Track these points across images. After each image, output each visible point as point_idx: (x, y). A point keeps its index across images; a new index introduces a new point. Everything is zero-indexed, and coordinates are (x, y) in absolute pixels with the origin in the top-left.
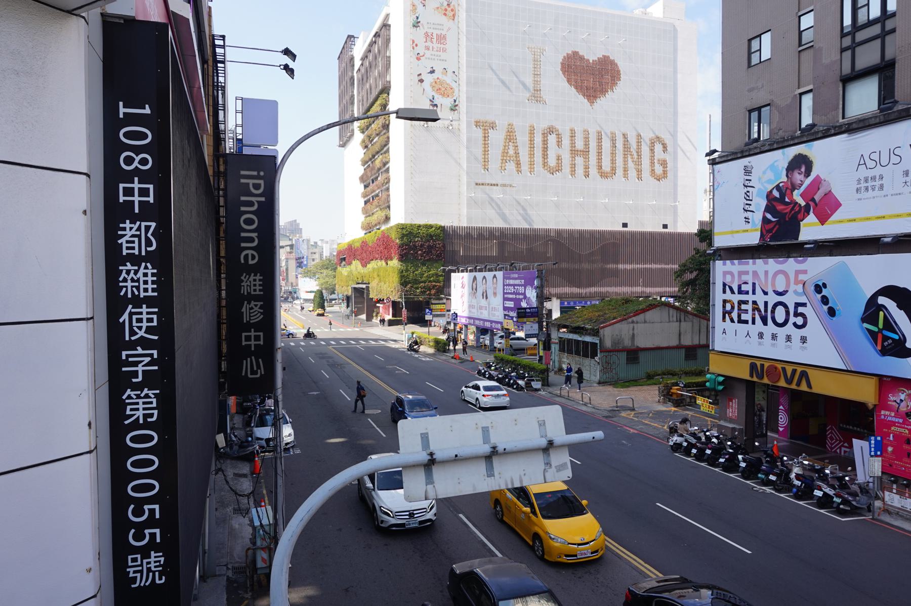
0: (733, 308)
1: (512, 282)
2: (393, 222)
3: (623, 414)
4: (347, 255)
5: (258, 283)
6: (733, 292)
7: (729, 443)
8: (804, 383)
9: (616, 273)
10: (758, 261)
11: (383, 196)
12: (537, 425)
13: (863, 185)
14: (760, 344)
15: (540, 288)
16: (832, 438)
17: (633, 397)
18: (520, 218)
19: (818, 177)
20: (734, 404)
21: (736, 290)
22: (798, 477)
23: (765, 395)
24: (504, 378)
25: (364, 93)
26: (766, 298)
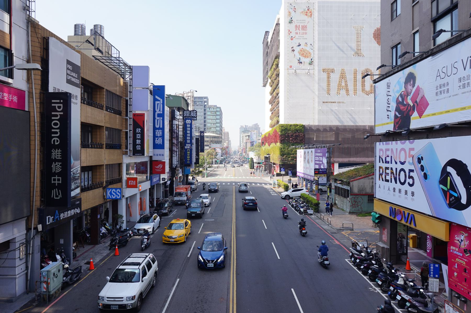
5: (59, 153)
18: (348, 120)
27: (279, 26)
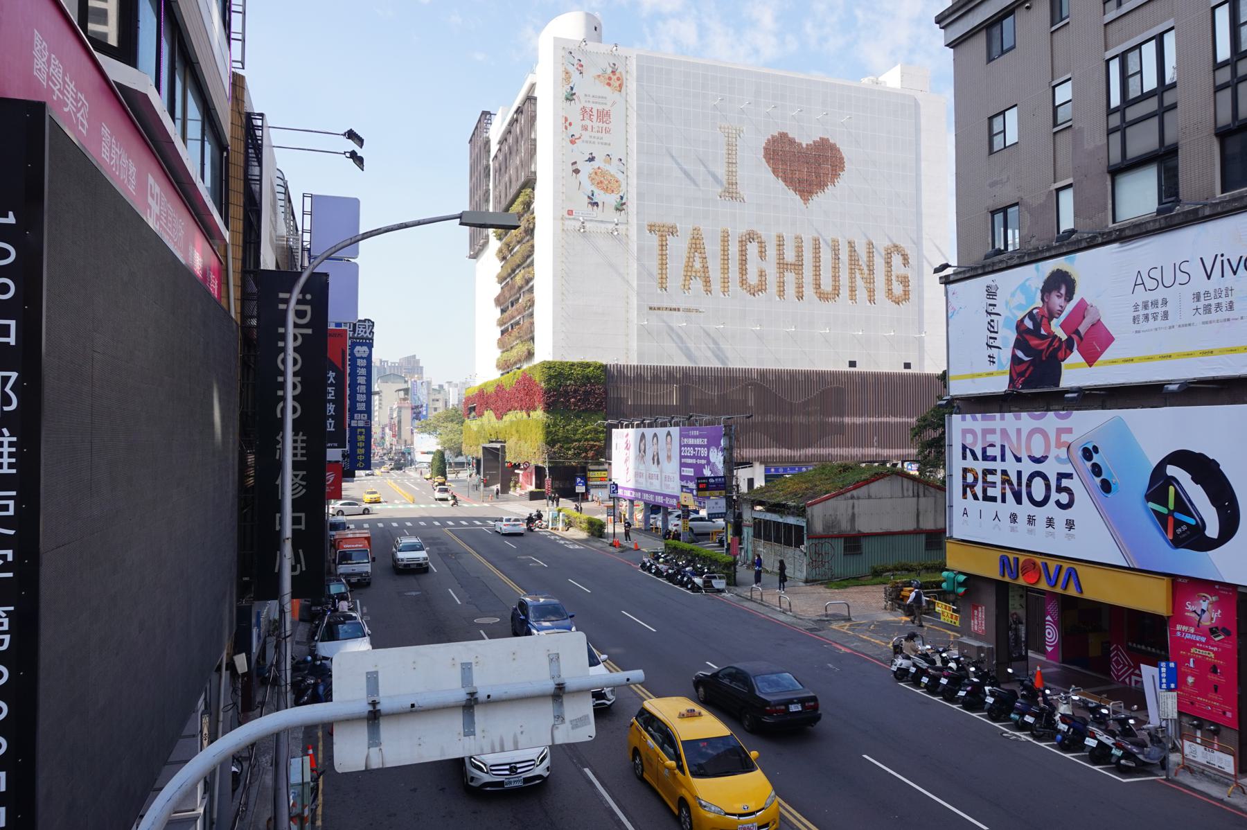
0: (976, 479)
1: (691, 441)
2: (538, 359)
3: (835, 626)
4: (478, 403)
6: (975, 458)
7: (973, 669)
8: (1072, 585)
9: (841, 428)
10: (1006, 415)
11: (525, 324)
12: (546, 661)
13: (1142, 312)
14: (1013, 530)
15: (728, 450)
16: (1118, 663)
17: (850, 602)
18: (709, 354)
19: (1082, 300)
20: (981, 613)
21: (979, 455)
22: (1064, 718)
23: (1023, 601)
24: (675, 574)
25: (502, 187)
26: (1019, 466)
27: (535, 104)
